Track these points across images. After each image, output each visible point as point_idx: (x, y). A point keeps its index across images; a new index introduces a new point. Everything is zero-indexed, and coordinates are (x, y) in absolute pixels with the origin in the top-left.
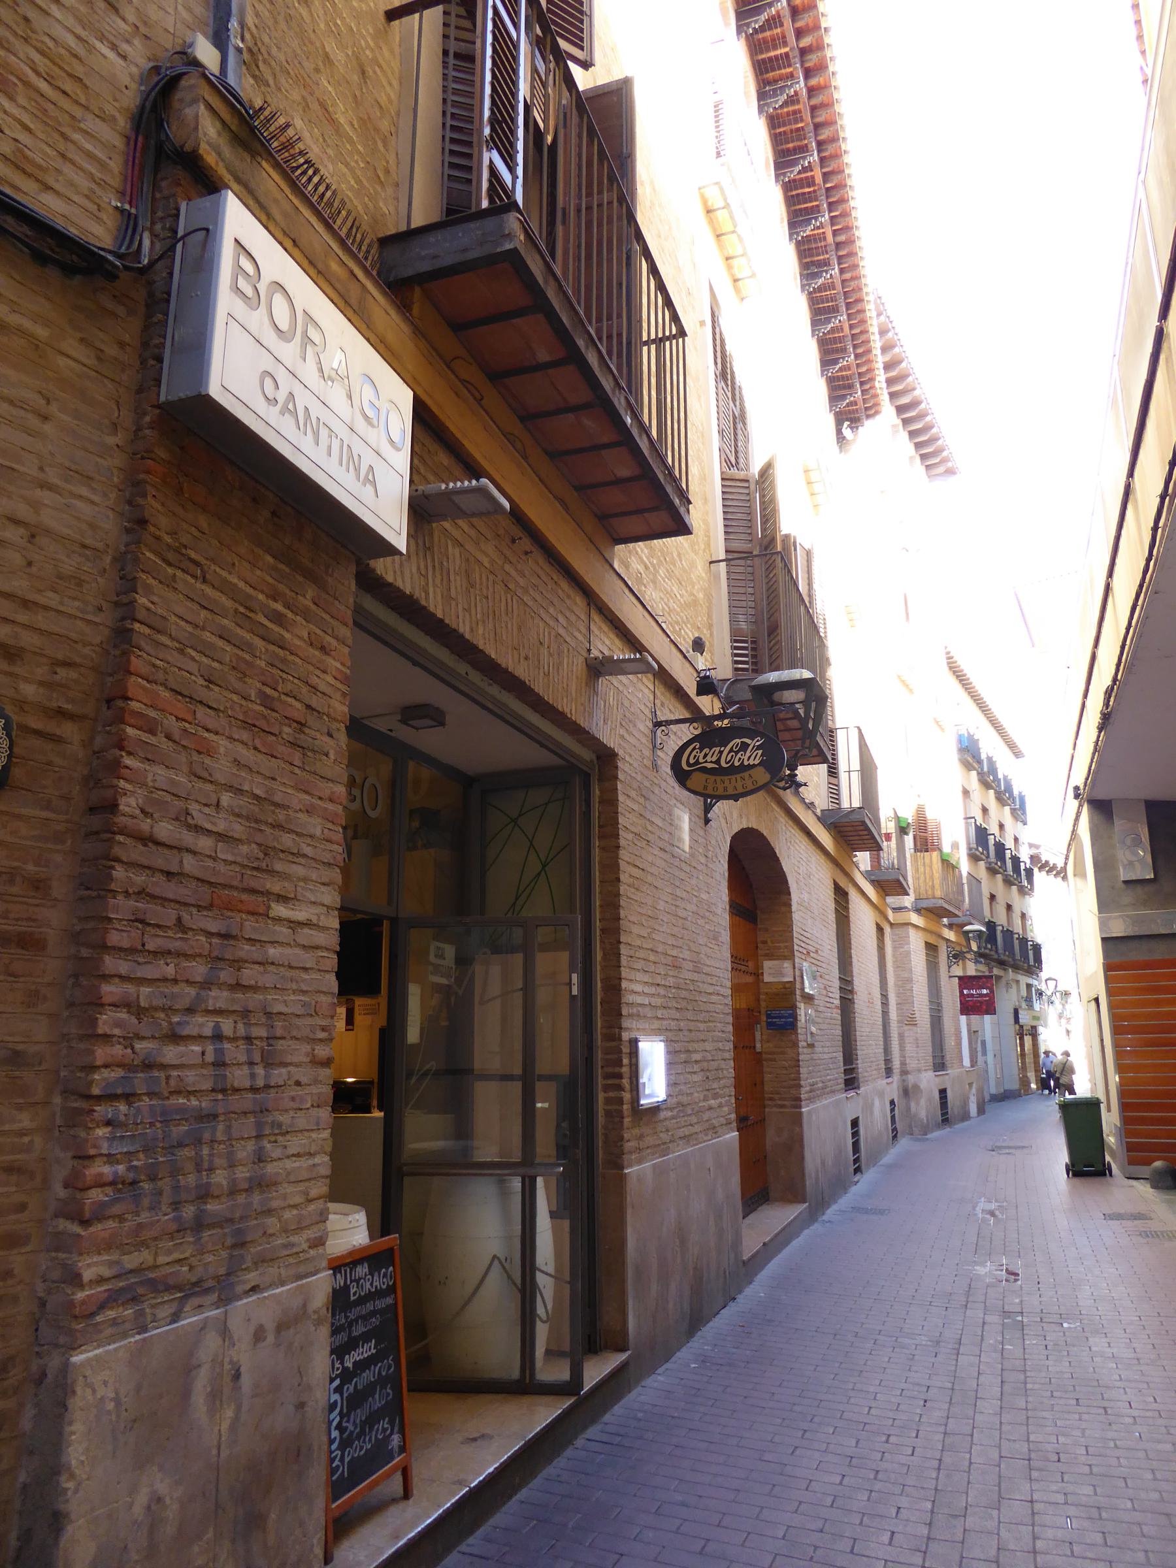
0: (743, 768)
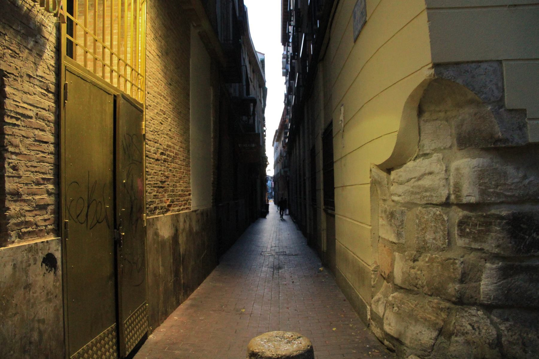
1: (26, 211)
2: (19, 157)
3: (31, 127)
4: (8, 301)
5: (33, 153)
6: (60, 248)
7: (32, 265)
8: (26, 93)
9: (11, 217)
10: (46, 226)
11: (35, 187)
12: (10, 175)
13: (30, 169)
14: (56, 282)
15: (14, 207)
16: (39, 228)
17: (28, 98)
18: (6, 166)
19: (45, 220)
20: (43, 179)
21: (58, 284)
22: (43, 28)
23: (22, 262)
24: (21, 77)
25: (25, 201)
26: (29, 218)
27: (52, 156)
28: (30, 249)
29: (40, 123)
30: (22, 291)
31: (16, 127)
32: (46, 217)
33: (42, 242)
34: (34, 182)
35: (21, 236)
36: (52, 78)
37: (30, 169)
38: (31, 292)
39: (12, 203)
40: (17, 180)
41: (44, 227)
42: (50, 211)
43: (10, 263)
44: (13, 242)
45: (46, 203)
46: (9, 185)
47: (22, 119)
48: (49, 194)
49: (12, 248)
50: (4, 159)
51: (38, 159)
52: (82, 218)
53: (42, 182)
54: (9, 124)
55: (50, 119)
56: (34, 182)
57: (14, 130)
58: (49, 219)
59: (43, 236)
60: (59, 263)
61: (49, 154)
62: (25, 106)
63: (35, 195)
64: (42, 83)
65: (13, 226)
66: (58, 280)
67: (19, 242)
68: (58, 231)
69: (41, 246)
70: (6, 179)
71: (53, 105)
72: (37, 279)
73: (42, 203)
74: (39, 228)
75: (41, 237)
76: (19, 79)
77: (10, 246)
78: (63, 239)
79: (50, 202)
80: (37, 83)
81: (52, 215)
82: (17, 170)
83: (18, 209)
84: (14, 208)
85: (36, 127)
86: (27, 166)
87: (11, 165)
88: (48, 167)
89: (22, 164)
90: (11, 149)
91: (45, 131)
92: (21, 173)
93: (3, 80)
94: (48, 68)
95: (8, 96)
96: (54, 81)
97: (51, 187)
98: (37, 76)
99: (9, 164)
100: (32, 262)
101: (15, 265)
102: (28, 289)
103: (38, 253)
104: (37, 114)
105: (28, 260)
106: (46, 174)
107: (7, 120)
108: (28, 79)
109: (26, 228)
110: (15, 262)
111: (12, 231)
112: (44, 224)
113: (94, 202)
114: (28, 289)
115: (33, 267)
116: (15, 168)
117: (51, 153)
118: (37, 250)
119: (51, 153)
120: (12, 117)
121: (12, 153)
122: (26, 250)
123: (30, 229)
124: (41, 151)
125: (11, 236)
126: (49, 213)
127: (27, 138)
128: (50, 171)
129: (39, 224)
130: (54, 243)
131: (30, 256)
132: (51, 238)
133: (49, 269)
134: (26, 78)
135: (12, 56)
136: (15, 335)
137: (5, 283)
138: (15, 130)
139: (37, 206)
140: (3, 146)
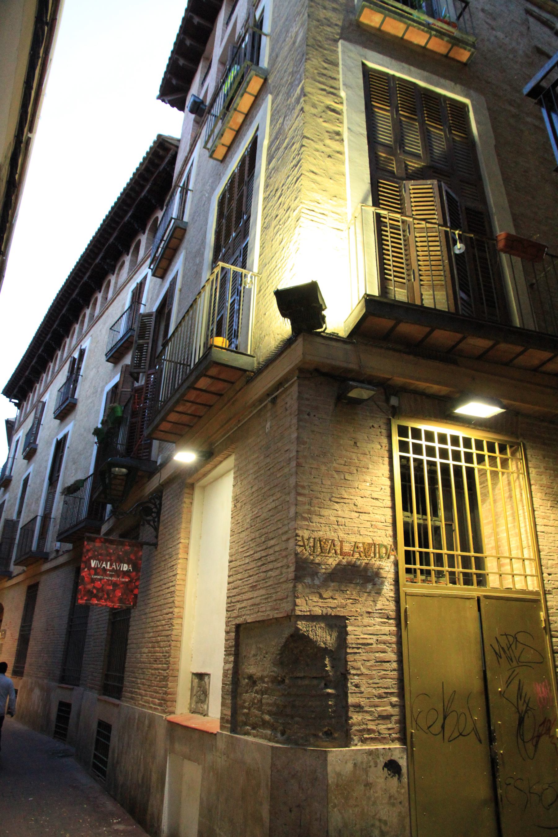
1: (368, 720)
2: (360, 678)
3: (372, 652)
4: (349, 792)
5: (374, 672)
6: (405, 757)
7: (373, 767)
8: (366, 626)
9: (353, 725)
10: (390, 734)
11: (377, 700)
12: (353, 691)
13: (372, 685)
14: (401, 789)
15: (356, 716)
16: (382, 736)
17: (368, 630)
18: (349, 685)
19: (389, 729)
20: (385, 693)
21: (403, 791)
22: (381, 570)
23: (362, 763)
24: (361, 615)
25: (367, 712)
26: (371, 726)
27: (395, 673)
28: (370, 753)
29: (381, 646)
30: (362, 787)
31: (358, 655)
32: (390, 726)
33: (384, 748)
34: (376, 696)
35: (364, 741)
36: (392, 606)
37: (372, 685)
38: (372, 791)
39: (355, 713)
40: (359, 695)
41: (388, 735)
42: (394, 721)
43: (351, 762)
44: (356, 745)
45: (389, 714)
46: (351, 700)
47: (363, 647)
48: (393, 705)
49: (353, 750)
50: (348, 680)
51: (379, 676)
52: (437, 728)
53: (384, 695)
54: (351, 653)
55: (390, 641)
56: (376, 696)
57: (355, 657)
58: (393, 728)
59: (387, 743)
60: (404, 770)
61: (391, 671)
62: (366, 636)
63: (377, 706)
64: (382, 614)
65: (356, 732)
66: (404, 787)
67: (361, 746)
68: (403, 740)
69: (383, 751)
70: (349, 695)
71: (395, 629)
72: (378, 780)
73: (385, 714)
74: (382, 736)
75: (384, 744)
76: (359, 618)
77: (353, 748)
78: (409, 748)
79: (393, 713)
80: (378, 615)
81: (398, 725)
82: (359, 687)
83: (360, 718)
84: (356, 717)
85: (377, 651)
86: (369, 684)
87: (354, 684)
88: (391, 683)
89: (363, 682)
90: (352, 672)
91: (387, 652)
92: (362, 689)
93: (346, 623)
94: (388, 600)
95: (349, 633)
96: (394, 608)
97: (394, 699)
98: (376, 610)
99: (352, 683)
100: (372, 764)
101: (355, 764)
102: (368, 788)
103: (378, 757)
104: (377, 640)
105: (369, 762)
106: (389, 688)
107: (349, 651)
108: (368, 615)
109: (369, 734)
110: (355, 761)
111: (355, 736)
112: (387, 732)
113: (454, 713)
114: (368, 788)
115: (373, 769)
116: (357, 686)
117: (394, 670)
118: (378, 754)
119: (394, 670)
120: (353, 648)
121: (354, 675)
122: (366, 753)
123: (372, 736)
124: (383, 670)
125: (354, 740)
126: (393, 723)
127: (368, 661)
128: (393, 686)
129: (381, 732)
130: (398, 751)
131: (370, 759)
132: (397, 745)
133: (392, 774)
134: (366, 615)
135: (352, 604)
136: (356, 824)
137: (346, 777)
138: (357, 657)
139: (379, 716)
140: (347, 670)
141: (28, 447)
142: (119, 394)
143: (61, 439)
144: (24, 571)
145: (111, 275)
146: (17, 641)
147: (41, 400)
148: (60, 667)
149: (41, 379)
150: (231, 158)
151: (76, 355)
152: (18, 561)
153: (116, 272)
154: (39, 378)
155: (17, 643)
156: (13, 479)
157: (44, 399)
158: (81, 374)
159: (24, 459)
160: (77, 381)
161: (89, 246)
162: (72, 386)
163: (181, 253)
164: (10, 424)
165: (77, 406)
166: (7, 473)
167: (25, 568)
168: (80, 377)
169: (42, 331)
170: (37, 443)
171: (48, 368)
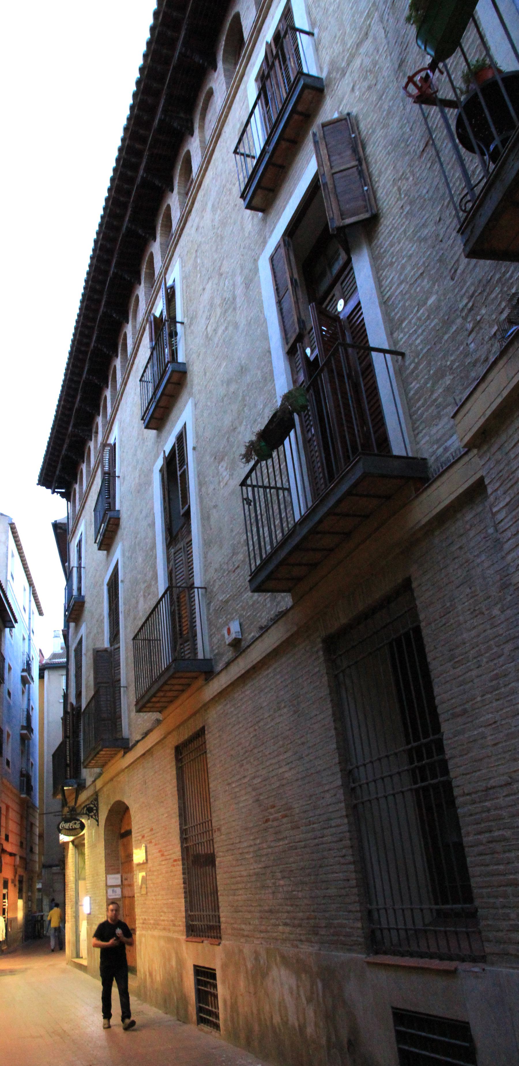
0: (75, 829)
141: (102, 522)
142: (329, 182)
143: (173, 451)
144: (158, 722)
145: (170, 193)
146: (180, 863)
147: (108, 442)
148: (357, 907)
149: (94, 430)
150: (262, 122)
151: (160, 308)
152: (141, 704)
153: (93, 439)
154: (91, 431)
155: (180, 868)
156: (87, 599)
157: (111, 441)
158: (179, 318)
159: (99, 549)
160: (176, 334)
161: (76, 328)
162: (166, 350)
163: (187, 402)
164: (61, 528)
165: (188, 375)
166: (75, 592)
167: (155, 716)
168: (178, 325)
169: (50, 459)
170: (117, 508)
171: (95, 426)
